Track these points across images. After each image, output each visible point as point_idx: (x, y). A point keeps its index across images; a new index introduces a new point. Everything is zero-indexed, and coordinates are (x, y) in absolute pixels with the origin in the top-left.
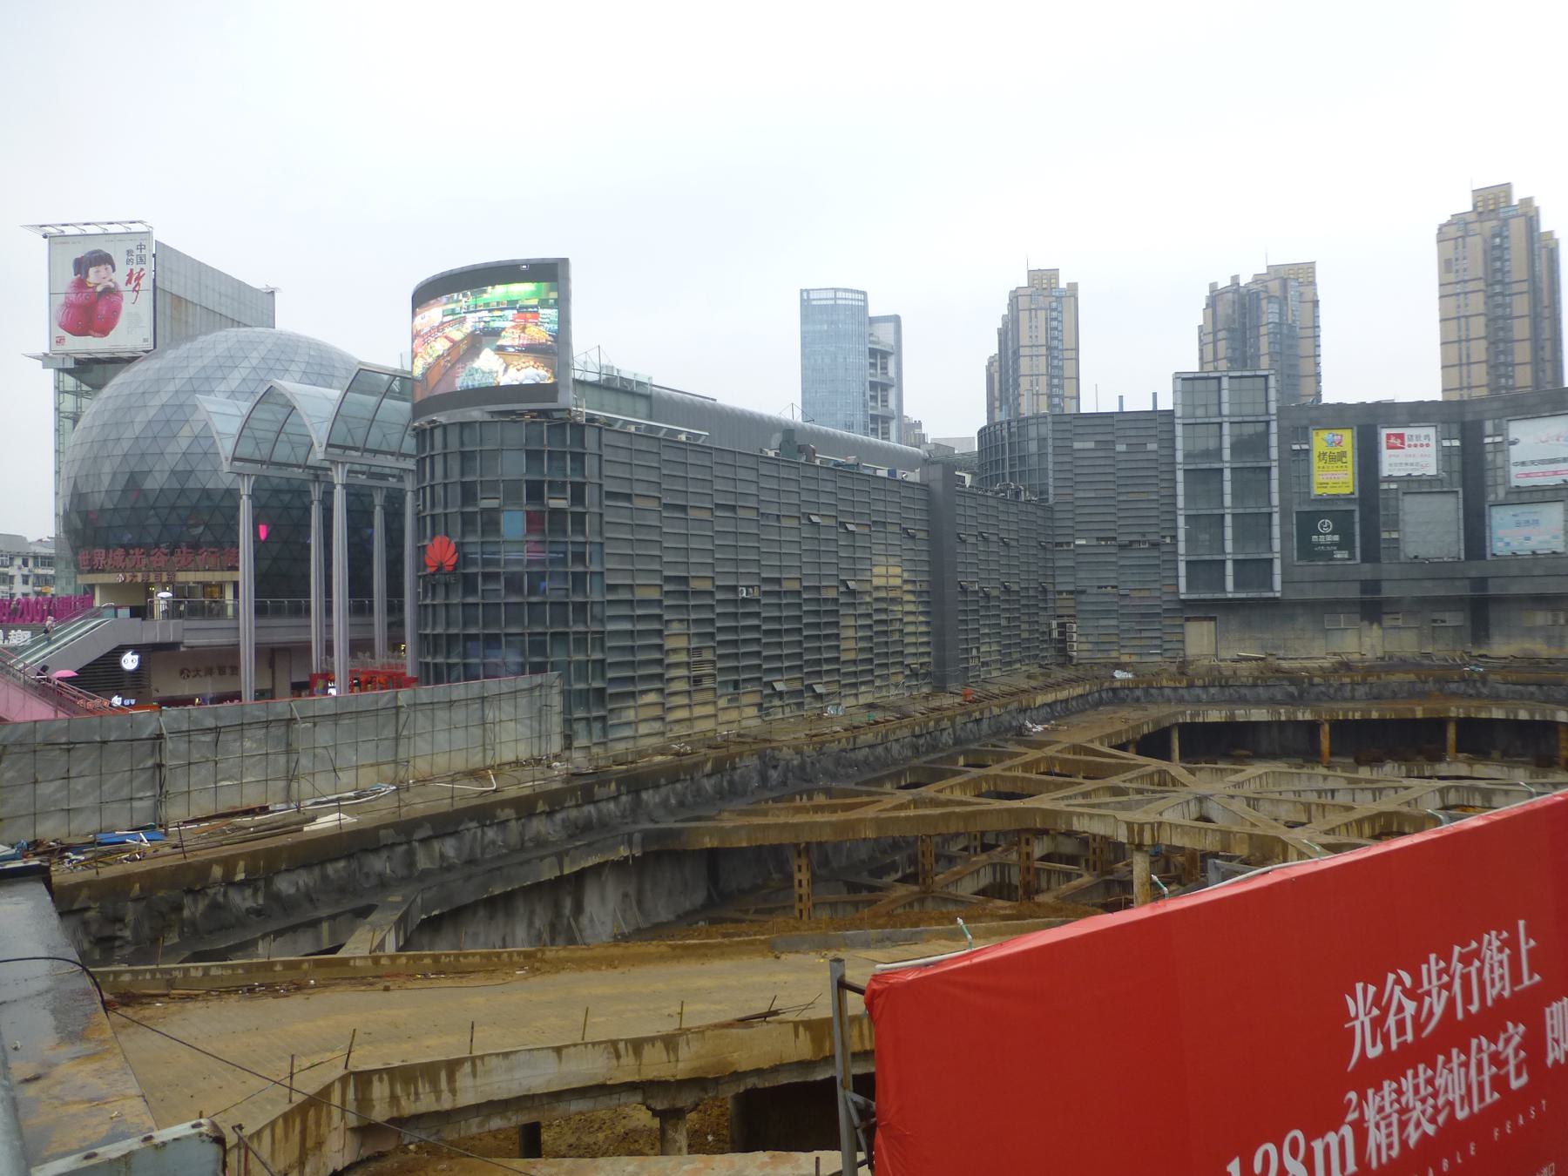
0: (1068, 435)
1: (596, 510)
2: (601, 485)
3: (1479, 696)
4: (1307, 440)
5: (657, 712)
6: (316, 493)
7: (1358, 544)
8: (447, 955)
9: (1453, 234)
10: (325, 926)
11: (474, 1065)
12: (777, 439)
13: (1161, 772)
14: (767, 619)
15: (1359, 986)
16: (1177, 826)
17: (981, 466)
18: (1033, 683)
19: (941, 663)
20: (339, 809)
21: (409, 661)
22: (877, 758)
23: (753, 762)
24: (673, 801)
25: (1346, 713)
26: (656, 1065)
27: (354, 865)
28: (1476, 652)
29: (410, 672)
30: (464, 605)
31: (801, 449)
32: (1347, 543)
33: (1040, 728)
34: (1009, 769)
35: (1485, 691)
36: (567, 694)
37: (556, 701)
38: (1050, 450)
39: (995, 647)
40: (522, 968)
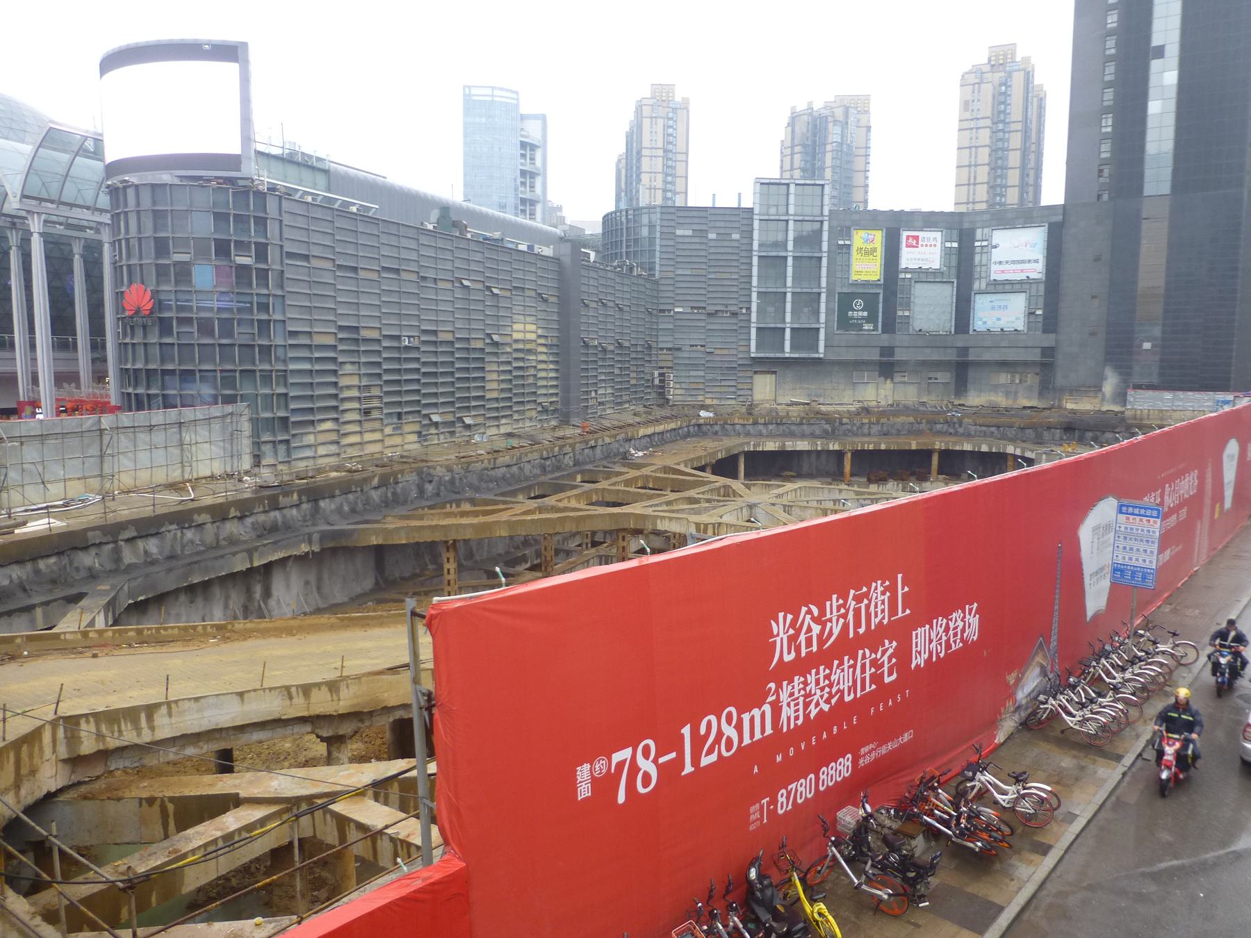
0: (672, 224)
1: (277, 267)
2: (282, 246)
3: (956, 434)
4: (849, 237)
5: (334, 437)
6: (14, 239)
7: (880, 320)
8: (149, 629)
9: (973, 80)
10: (39, 611)
11: (169, 708)
12: (435, 215)
13: (726, 487)
14: (425, 364)
15: (781, 615)
16: (732, 526)
17: (604, 245)
18: (637, 419)
19: (566, 402)
20: (48, 515)
21: (112, 390)
22: (513, 476)
23: (413, 477)
24: (346, 508)
25: (863, 445)
26: (322, 703)
27: (65, 560)
28: (957, 402)
29: (114, 400)
30: (161, 344)
31: (455, 224)
32: (872, 318)
33: (640, 454)
34: (614, 484)
35: (961, 430)
36: (255, 422)
37: (246, 427)
38: (658, 235)
39: (610, 391)
40: (214, 637)
